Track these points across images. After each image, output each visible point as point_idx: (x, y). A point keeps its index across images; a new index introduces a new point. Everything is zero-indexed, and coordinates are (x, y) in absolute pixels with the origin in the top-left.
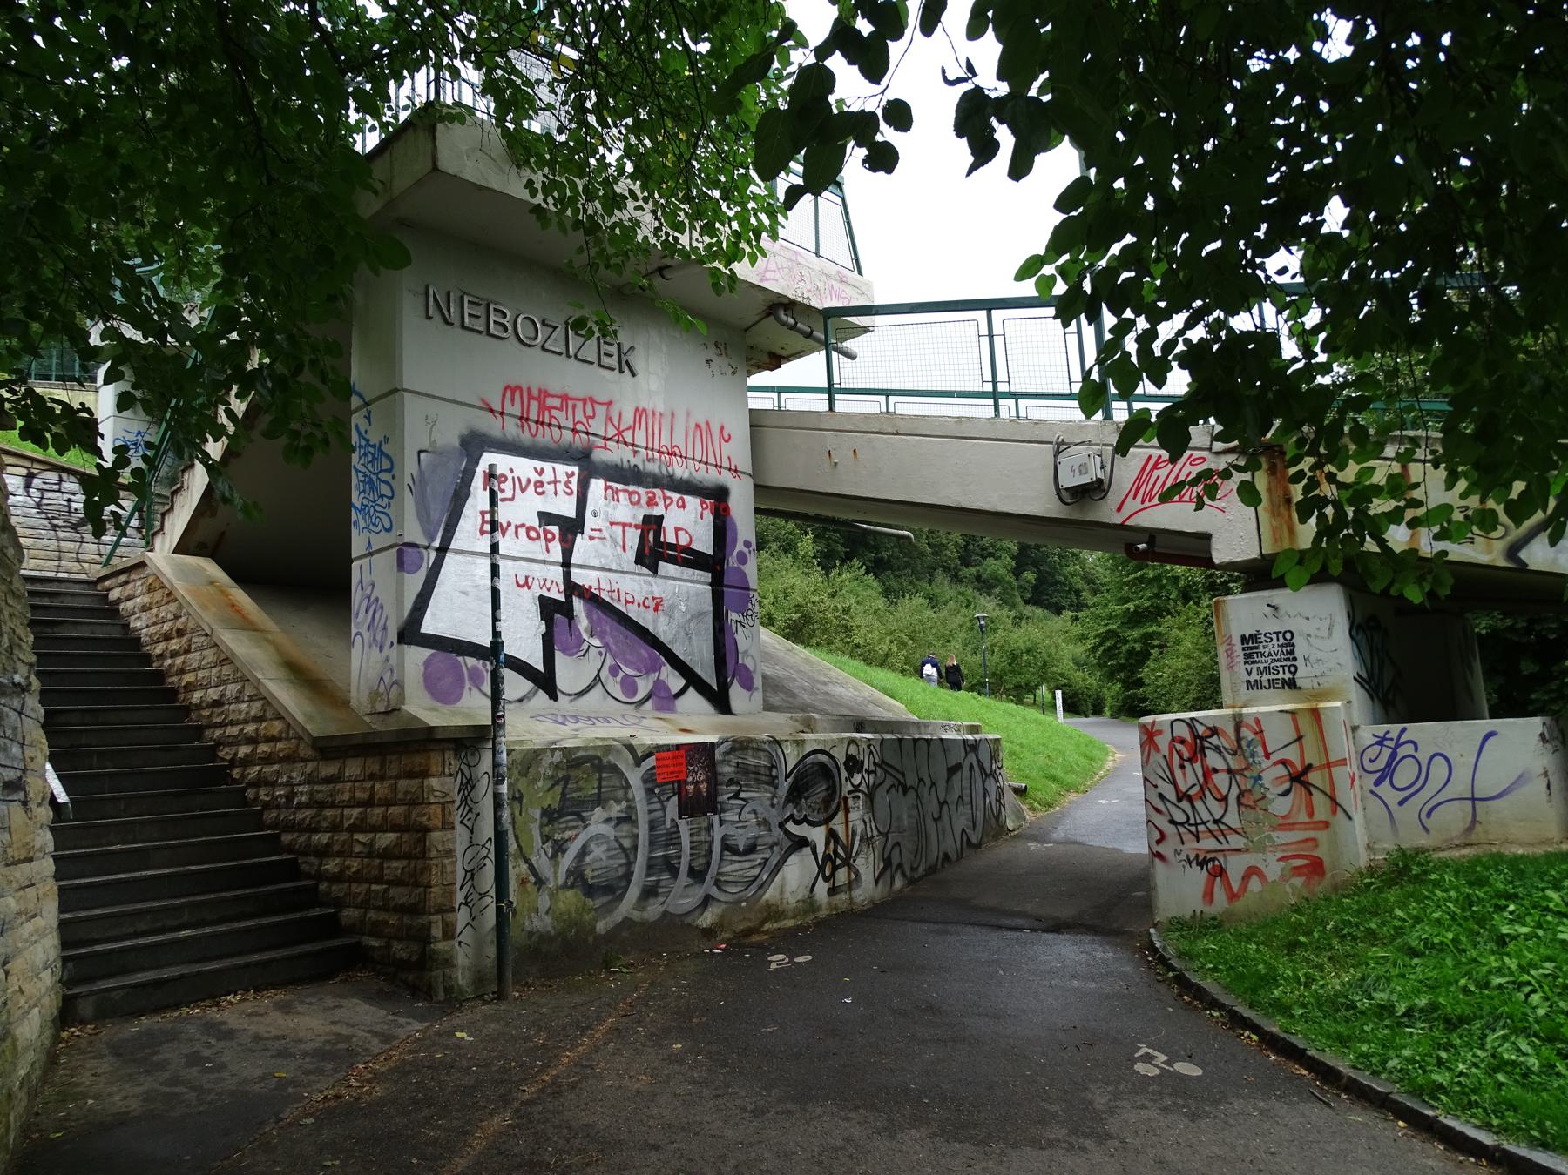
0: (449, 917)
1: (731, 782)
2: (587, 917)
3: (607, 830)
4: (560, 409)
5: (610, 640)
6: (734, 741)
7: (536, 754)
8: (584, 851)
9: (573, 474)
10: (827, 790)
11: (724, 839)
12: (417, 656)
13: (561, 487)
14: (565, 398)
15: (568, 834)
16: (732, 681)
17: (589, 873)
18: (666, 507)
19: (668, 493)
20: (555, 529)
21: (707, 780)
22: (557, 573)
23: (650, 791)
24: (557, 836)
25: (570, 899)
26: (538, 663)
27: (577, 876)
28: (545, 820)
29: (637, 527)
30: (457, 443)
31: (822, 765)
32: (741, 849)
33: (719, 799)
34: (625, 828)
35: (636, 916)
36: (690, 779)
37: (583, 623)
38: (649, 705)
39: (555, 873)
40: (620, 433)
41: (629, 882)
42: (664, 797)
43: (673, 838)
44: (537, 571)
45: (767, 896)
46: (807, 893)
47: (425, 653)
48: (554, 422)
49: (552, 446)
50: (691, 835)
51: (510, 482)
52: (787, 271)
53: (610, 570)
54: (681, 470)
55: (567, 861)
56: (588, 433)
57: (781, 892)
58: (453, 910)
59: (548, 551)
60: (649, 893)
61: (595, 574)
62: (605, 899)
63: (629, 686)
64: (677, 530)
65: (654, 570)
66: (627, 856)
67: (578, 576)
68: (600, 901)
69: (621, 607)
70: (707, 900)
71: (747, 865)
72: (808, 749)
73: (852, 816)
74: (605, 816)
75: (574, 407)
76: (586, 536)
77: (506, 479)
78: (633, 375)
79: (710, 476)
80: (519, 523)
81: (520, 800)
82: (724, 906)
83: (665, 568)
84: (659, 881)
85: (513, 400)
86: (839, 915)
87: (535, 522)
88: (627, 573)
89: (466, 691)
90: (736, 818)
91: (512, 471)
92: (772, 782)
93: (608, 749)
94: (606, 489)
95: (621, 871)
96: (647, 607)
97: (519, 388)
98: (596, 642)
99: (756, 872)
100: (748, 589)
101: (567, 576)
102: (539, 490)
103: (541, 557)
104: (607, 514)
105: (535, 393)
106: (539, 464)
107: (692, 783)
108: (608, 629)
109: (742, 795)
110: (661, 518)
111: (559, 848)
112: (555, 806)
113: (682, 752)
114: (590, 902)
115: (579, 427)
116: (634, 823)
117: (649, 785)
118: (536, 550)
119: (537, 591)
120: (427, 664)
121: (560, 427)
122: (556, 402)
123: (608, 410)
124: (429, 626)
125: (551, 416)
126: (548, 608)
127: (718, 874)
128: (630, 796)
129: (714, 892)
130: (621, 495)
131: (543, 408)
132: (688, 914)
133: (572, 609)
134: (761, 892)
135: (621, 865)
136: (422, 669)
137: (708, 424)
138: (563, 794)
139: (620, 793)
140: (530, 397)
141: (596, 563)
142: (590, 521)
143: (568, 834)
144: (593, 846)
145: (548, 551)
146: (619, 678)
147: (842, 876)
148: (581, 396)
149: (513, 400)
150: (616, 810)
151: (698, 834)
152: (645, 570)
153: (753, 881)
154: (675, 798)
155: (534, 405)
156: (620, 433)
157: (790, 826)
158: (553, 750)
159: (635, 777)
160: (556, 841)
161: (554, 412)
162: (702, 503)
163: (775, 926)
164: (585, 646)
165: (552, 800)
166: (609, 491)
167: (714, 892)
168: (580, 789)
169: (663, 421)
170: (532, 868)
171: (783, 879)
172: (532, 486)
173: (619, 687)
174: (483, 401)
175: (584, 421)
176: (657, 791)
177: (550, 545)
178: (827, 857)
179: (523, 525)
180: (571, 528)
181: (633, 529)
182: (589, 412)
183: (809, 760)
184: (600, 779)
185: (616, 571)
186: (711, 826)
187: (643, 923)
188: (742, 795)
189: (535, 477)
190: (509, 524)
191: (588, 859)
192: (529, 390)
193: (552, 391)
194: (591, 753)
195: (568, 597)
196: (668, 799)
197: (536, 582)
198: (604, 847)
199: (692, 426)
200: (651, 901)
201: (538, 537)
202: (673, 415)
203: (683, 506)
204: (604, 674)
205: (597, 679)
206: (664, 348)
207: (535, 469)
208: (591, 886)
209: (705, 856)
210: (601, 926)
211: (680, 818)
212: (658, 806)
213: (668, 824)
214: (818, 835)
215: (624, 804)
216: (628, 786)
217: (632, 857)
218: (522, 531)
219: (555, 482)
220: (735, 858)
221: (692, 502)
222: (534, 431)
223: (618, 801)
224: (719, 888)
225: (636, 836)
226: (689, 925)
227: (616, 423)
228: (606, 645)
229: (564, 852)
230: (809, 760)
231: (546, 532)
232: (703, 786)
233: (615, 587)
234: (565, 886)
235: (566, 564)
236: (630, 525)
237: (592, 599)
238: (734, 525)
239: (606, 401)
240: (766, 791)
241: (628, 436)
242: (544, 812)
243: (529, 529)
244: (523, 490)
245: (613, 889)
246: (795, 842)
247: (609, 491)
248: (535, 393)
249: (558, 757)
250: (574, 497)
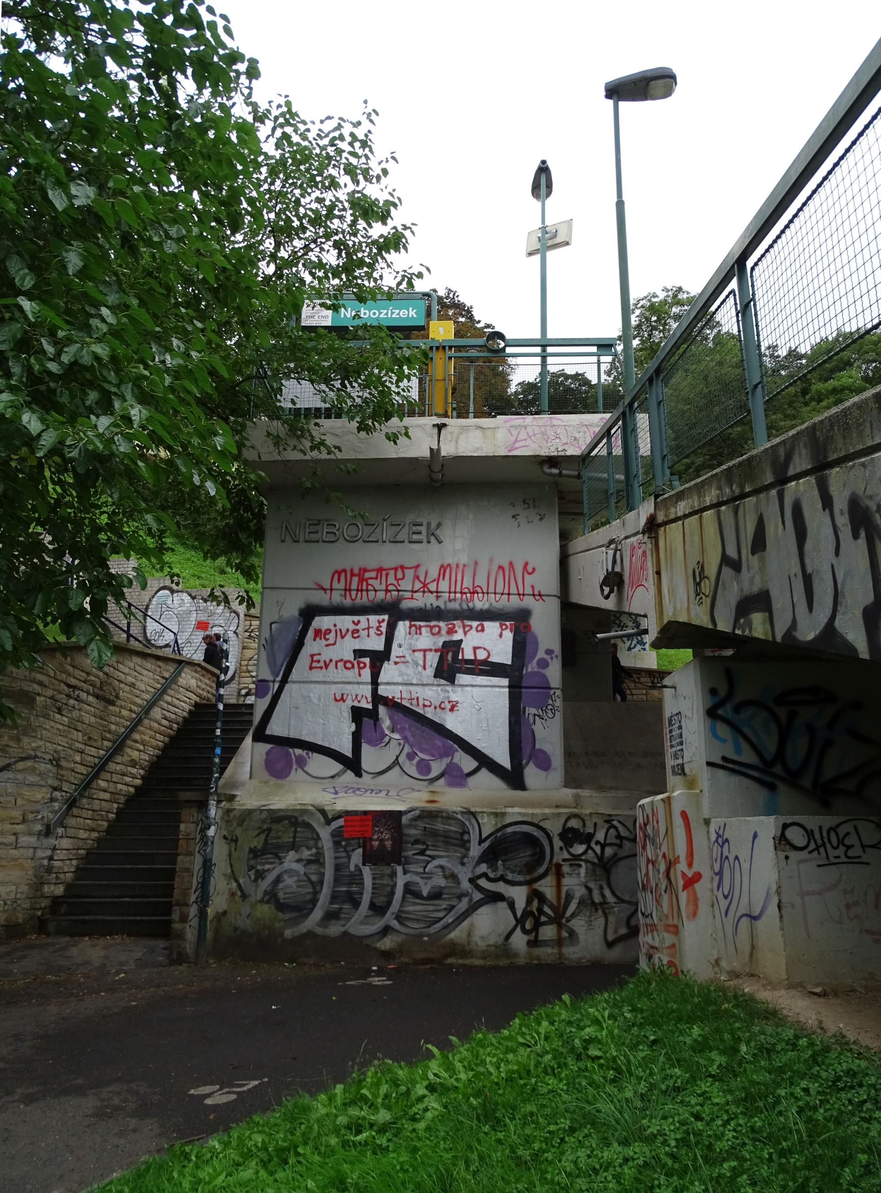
0: (185, 909)
1: (417, 842)
2: (277, 925)
3: (299, 867)
4: (376, 578)
5: (409, 735)
6: (423, 811)
7: (250, 812)
8: (278, 880)
10: (533, 855)
11: (407, 885)
13: (372, 632)
14: (380, 570)
15: (267, 866)
16: (527, 763)
17: (281, 895)
18: (465, 633)
20: (367, 660)
21: (393, 839)
22: (367, 690)
23: (337, 844)
24: (259, 867)
25: (266, 911)
27: (271, 896)
28: (251, 855)
30: (296, 613)
31: (528, 836)
32: (425, 894)
33: (404, 854)
34: (313, 868)
35: (319, 931)
36: (375, 837)
37: (386, 723)
38: (442, 781)
39: (256, 892)
41: (314, 906)
42: (348, 849)
43: (357, 878)
45: (452, 935)
46: (500, 941)
47: (365, 748)
48: (370, 588)
49: (368, 604)
50: (374, 879)
52: (539, 436)
53: (412, 684)
54: (480, 603)
55: (265, 884)
56: (398, 591)
57: (469, 935)
58: (187, 905)
60: (331, 916)
61: (400, 688)
62: (293, 915)
63: (423, 767)
64: (475, 649)
65: (451, 680)
66: (314, 888)
67: (382, 691)
68: (288, 916)
70: (386, 930)
71: (431, 908)
72: (509, 820)
73: (567, 881)
74: (297, 857)
75: (387, 575)
76: (391, 662)
78: (440, 542)
81: (236, 841)
82: (404, 937)
83: (463, 678)
84: (341, 909)
86: (539, 966)
89: (293, 771)
90: (421, 870)
92: (464, 844)
93: (304, 812)
95: (308, 897)
96: (443, 709)
97: (345, 571)
98: (396, 736)
99: (441, 915)
100: (550, 688)
101: (375, 691)
104: (410, 644)
105: (356, 571)
106: (356, 618)
107: (376, 840)
109: (428, 852)
110: (461, 641)
111: (260, 875)
112: (260, 847)
113: (369, 817)
114: (280, 915)
116: (322, 865)
117: (337, 839)
119: (349, 703)
121: (376, 591)
122: (373, 574)
125: (368, 585)
126: (357, 714)
127: (399, 911)
128: (320, 845)
129: (395, 924)
130: (423, 630)
131: (362, 580)
132: (367, 937)
133: (378, 714)
134: (444, 931)
135: (309, 893)
137: (511, 564)
138: (266, 840)
139: (312, 843)
140: (352, 575)
141: (400, 680)
142: (395, 651)
143: (267, 866)
144: (285, 877)
145: (360, 675)
146: (415, 762)
147: (548, 932)
148: (393, 565)
150: (306, 854)
151: (381, 878)
152: (442, 682)
153: (436, 922)
154: (360, 850)
155: (355, 580)
156: (425, 585)
157: (483, 882)
158: (261, 811)
159: (325, 833)
160: (257, 871)
161: (370, 582)
162: (501, 626)
163: (461, 961)
164: (387, 739)
165: (258, 843)
166: (413, 629)
167: (395, 924)
168: (279, 838)
169: (466, 570)
170: (239, 886)
171: (472, 924)
172: (350, 633)
173: (414, 768)
174: (317, 584)
175: (395, 582)
176: (343, 843)
177: (362, 671)
178: (527, 913)
180: (379, 659)
181: (433, 653)
182: (400, 575)
183: (510, 830)
184: (295, 832)
185: (417, 685)
186: (394, 874)
187: (324, 937)
188: (428, 852)
189: (352, 627)
190: (331, 661)
191: (281, 886)
192: (352, 570)
193: (369, 567)
194: (289, 814)
196: (353, 850)
198: (295, 878)
199: (495, 567)
200: (333, 922)
201: (353, 666)
202: (476, 563)
203: (483, 630)
205: (396, 762)
206: (471, 516)
208: (282, 904)
209: (387, 896)
210: (288, 933)
211: (364, 864)
212: (344, 854)
213: (352, 868)
214: (519, 895)
215: (314, 851)
216: (318, 838)
217: (318, 888)
218: (340, 664)
219: (368, 628)
220: (417, 901)
221: (492, 627)
222: (354, 597)
223: (309, 848)
224: (400, 922)
226: (368, 946)
227: (422, 579)
228: (405, 738)
229: (263, 879)
230: (510, 830)
231: (359, 663)
232: (388, 844)
234: (261, 901)
235: (375, 683)
236: (431, 650)
237: (393, 705)
240: (456, 851)
241: (433, 587)
244: (343, 637)
245: (302, 909)
246: (486, 896)
247: (413, 629)
248: (356, 571)
249: (264, 815)
250: (383, 637)
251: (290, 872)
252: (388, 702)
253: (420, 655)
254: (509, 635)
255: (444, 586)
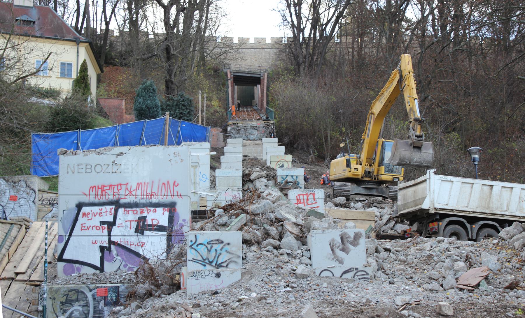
3: (80, 308)
4: (109, 190)
8: (72, 313)
9: (112, 208)
12: (61, 265)
15: (67, 308)
18: (148, 213)
19: (149, 208)
21: (116, 296)
22: (106, 239)
23: (94, 299)
24: (64, 309)
26: (99, 265)
28: (61, 304)
29: (136, 221)
30: (74, 206)
34: (85, 308)
36: (109, 296)
40: (130, 192)
44: (99, 239)
47: (106, 264)
51: (91, 214)
54: (154, 200)
56: (119, 195)
59: (103, 232)
64: (152, 220)
65: (142, 233)
66: (86, 315)
67: (112, 239)
69: (129, 246)
75: (114, 188)
77: (90, 214)
79: (169, 199)
80: (93, 225)
81: (55, 299)
83: (147, 233)
85: (93, 191)
87: (99, 224)
88: (131, 236)
91: (92, 211)
94: (124, 211)
96: (139, 246)
97: (95, 187)
102: (101, 215)
103: (101, 235)
105: (100, 187)
106: (101, 207)
108: (123, 253)
110: (146, 216)
115: (115, 194)
116: (89, 307)
118: (99, 232)
119: (99, 244)
120: (64, 266)
122: (108, 188)
123: (126, 186)
124: (65, 257)
125: (105, 193)
130: (130, 212)
136: (63, 268)
137: (168, 182)
138: (66, 298)
140: (98, 188)
141: (120, 234)
142: (118, 222)
143: (67, 308)
144: (75, 312)
145: (103, 232)
149: (93, 191)
150: (82, 303)
156: (130, 192)
160: (64, 310)
161: (106, 191)
162: (164, 209)
164: (115, 259)
165: (64, 300)
166: (126, 211)
169: (149, 185)
172: (98, 214)
179: (95, 226)
180: (111, 225)
181: (134, 222)
182: (119, 188)
185: (127, 236)
189: (99, 211)
190: (90, 226)
191: (73, 315)
192: (98, 186)
193: (106, 185)
195: (110, 245)
197: (99, 242)
198: (78, 312)
199: (161, 184)
201: (100, 229)
204: (121, 267)
207: (100, 209)
215: (85, 302)
216: (87, 297)
217: (87, 316)
218: (94, 228)
219: (106, 212)
221: (160, 210)
223: (83, 301)
225: (89, 310)
228: (123, 259)
229: (66, 313)
231: (102, 227)
233: (126, 241)
235: (109, 235)
236: (133, 221)
238: (178, 215)
239: (126, 183)
241: (134, 193)
242: (61, 303)
243: (96, 227)
244: (95, 216)
250: (113, 215)
251: (76, 310)
252: (114, 243)
253: (128, 223)
254: (167, 214)
255: (139, 192)
